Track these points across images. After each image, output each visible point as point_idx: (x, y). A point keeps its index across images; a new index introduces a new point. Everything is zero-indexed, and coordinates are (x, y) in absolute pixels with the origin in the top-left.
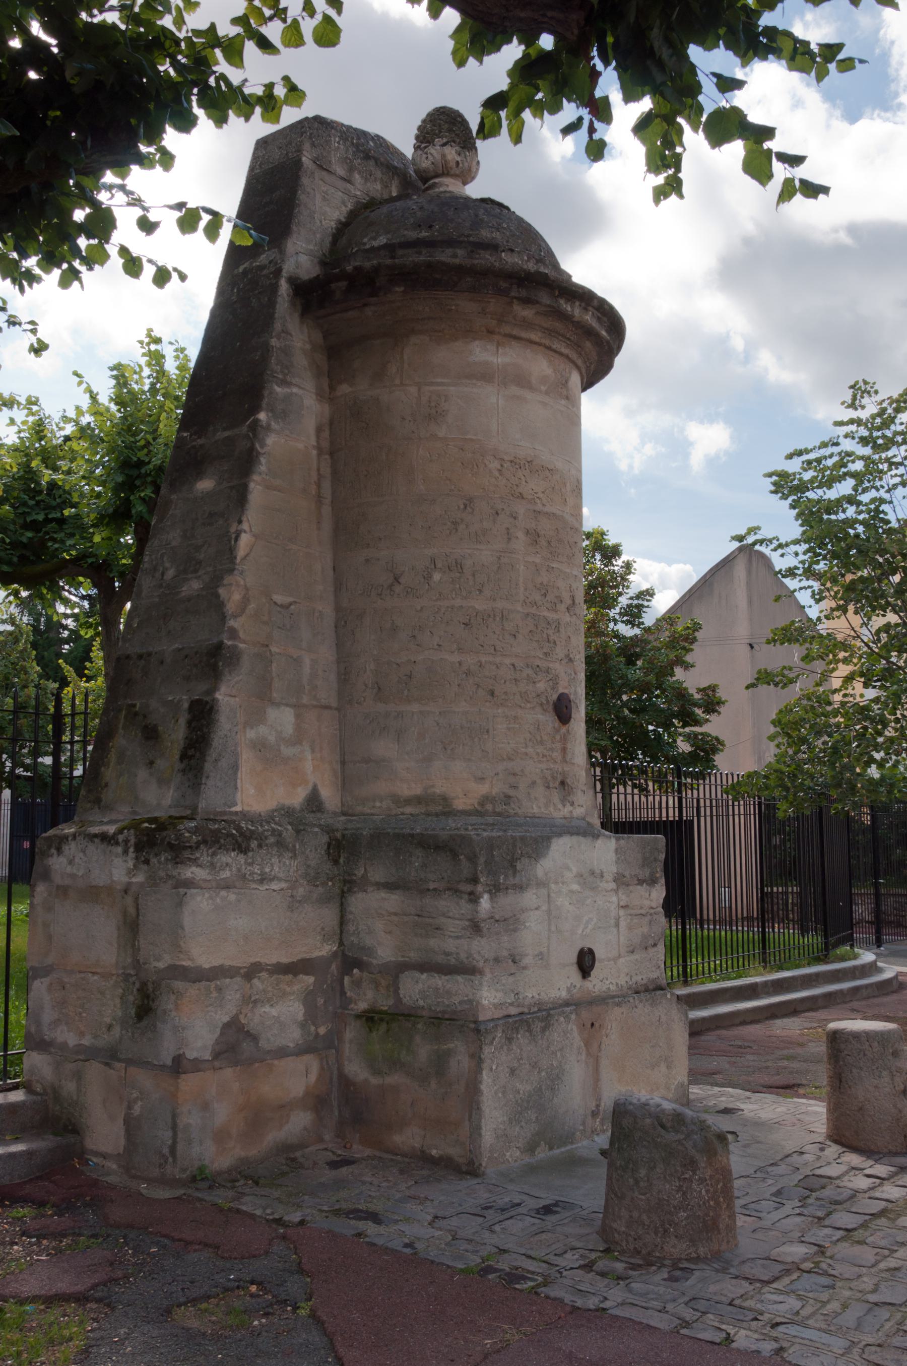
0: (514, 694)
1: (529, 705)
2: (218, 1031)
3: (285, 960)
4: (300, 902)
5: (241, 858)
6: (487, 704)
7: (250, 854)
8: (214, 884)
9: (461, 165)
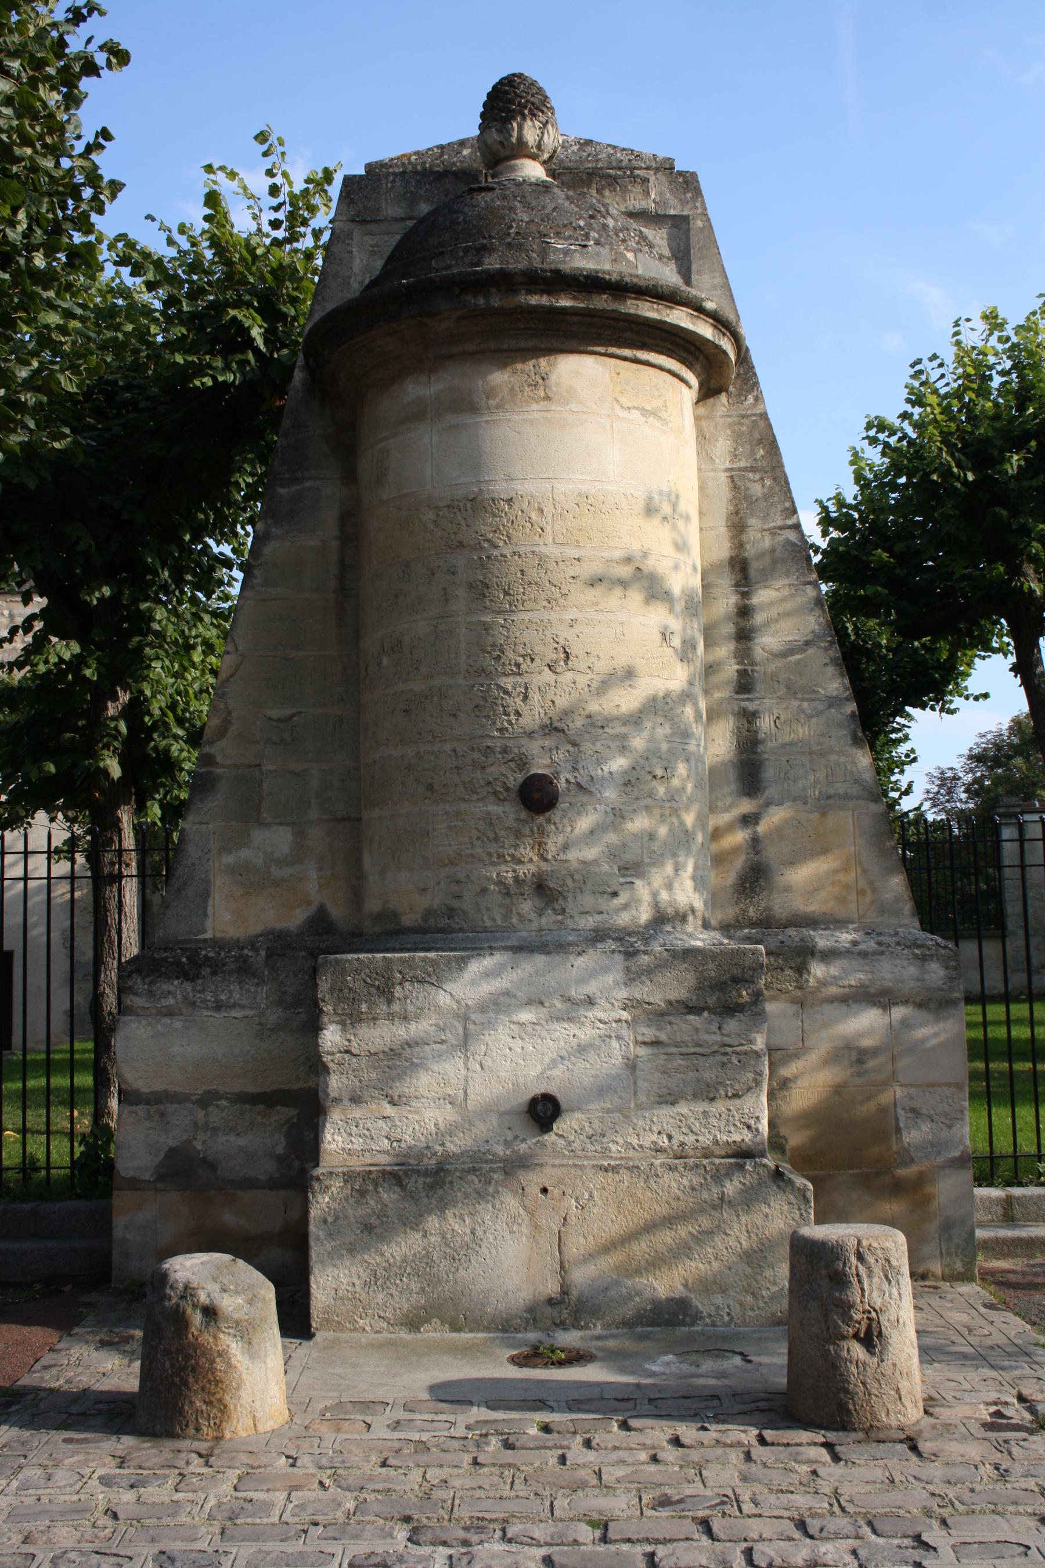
0: (456, 785)
1: (475, 797)
2: (162, 1154)
3: (252, 1089)
4: (272, 1030)
5: (188, 987)
6: (427, 801)
7: (200, 982)
8: (154, 1011)
9: (506, 144)
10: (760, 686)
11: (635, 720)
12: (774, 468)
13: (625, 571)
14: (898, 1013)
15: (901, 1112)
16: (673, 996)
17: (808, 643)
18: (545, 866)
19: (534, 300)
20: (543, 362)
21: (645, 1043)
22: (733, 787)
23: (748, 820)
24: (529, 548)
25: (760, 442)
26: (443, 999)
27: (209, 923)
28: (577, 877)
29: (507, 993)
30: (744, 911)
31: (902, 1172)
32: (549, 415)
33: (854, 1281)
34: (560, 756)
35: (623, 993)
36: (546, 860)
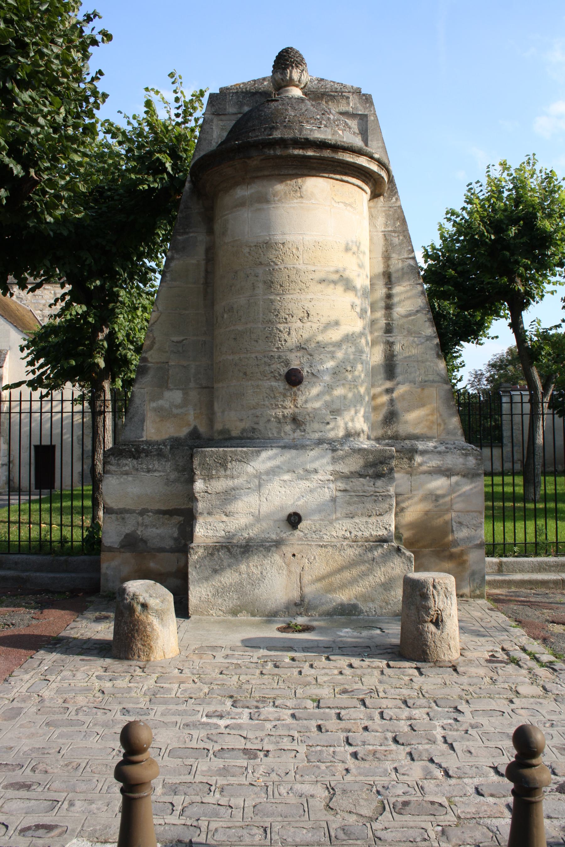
2: (123, 536)
5: (135, 462)
10: (395, 331)
11: (338, 345)
12: (404, 231)
13: (335, 277)
14: (454, 479)
15: (454, 523)
16: (353, 469)
17: (417, 311)
18: (297, 410)
19: (296, 152)
20: (300, 180)
21: (340, 490)
22: (382, 376)
23: (389, 391)
24: (292, 266)
25: (398, 219)
26: (250, 469)
27: (144, 433)
28: (311, 415)
29: (278, 467)
30: (386, 432)
31: (454, 550)
32: (302, 205)
33: (431, 597)
34: (304, 360)
35: (330, 468)
36: (297, 407)
